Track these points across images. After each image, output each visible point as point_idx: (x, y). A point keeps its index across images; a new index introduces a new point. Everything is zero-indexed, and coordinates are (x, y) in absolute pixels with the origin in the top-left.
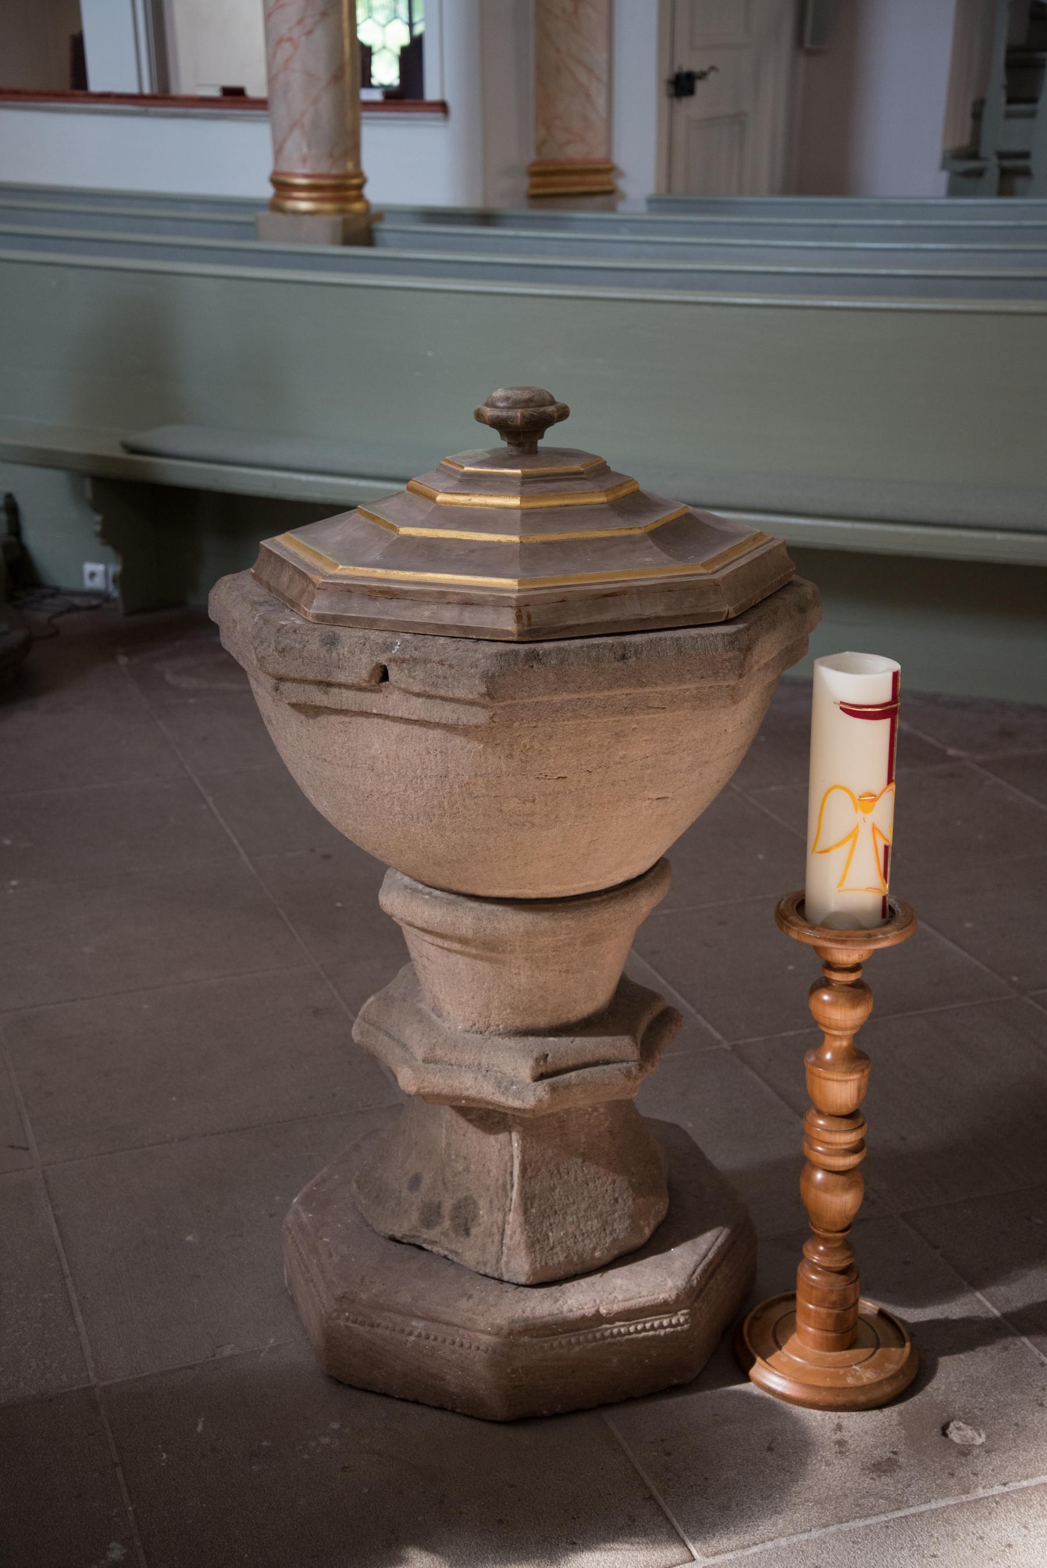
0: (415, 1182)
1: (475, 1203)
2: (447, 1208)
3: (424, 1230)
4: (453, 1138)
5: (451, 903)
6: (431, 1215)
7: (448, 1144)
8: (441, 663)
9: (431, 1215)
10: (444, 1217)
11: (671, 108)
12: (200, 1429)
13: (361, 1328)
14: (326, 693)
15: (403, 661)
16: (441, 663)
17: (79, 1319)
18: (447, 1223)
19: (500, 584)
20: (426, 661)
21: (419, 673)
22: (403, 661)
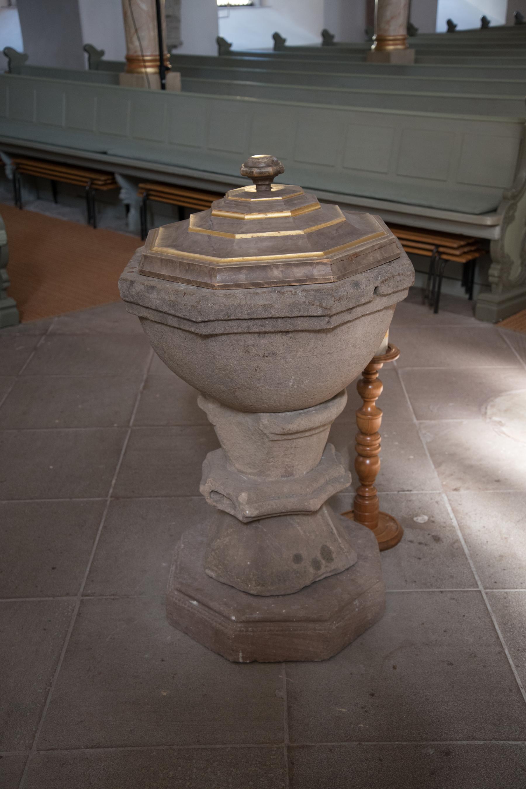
0: (298, 558)
1: (326, 546)
2: (319, 557)
3: (319, 572)
4: (305, 527)
5: (326, 408)
6: (316, 565)
7: (304, 532)
8: (399, 274)
9: (316, 565)
10: (320, 561)
11: (269, 7)
12: (344, 710)
13: (341, 623)
14: (350, 313)
15: (386, 281)
16: (399, 274)
17: (218, 746)
18: (323, 562)
19: (271, 258)
20: (394, 276)
21: (391, 284)
22: (386, 281)
